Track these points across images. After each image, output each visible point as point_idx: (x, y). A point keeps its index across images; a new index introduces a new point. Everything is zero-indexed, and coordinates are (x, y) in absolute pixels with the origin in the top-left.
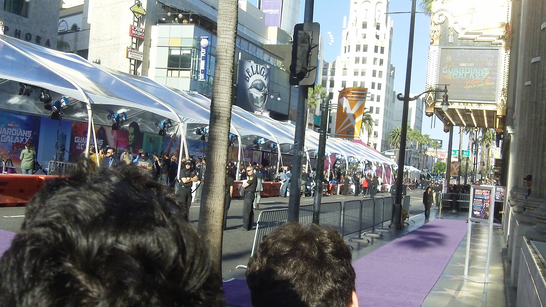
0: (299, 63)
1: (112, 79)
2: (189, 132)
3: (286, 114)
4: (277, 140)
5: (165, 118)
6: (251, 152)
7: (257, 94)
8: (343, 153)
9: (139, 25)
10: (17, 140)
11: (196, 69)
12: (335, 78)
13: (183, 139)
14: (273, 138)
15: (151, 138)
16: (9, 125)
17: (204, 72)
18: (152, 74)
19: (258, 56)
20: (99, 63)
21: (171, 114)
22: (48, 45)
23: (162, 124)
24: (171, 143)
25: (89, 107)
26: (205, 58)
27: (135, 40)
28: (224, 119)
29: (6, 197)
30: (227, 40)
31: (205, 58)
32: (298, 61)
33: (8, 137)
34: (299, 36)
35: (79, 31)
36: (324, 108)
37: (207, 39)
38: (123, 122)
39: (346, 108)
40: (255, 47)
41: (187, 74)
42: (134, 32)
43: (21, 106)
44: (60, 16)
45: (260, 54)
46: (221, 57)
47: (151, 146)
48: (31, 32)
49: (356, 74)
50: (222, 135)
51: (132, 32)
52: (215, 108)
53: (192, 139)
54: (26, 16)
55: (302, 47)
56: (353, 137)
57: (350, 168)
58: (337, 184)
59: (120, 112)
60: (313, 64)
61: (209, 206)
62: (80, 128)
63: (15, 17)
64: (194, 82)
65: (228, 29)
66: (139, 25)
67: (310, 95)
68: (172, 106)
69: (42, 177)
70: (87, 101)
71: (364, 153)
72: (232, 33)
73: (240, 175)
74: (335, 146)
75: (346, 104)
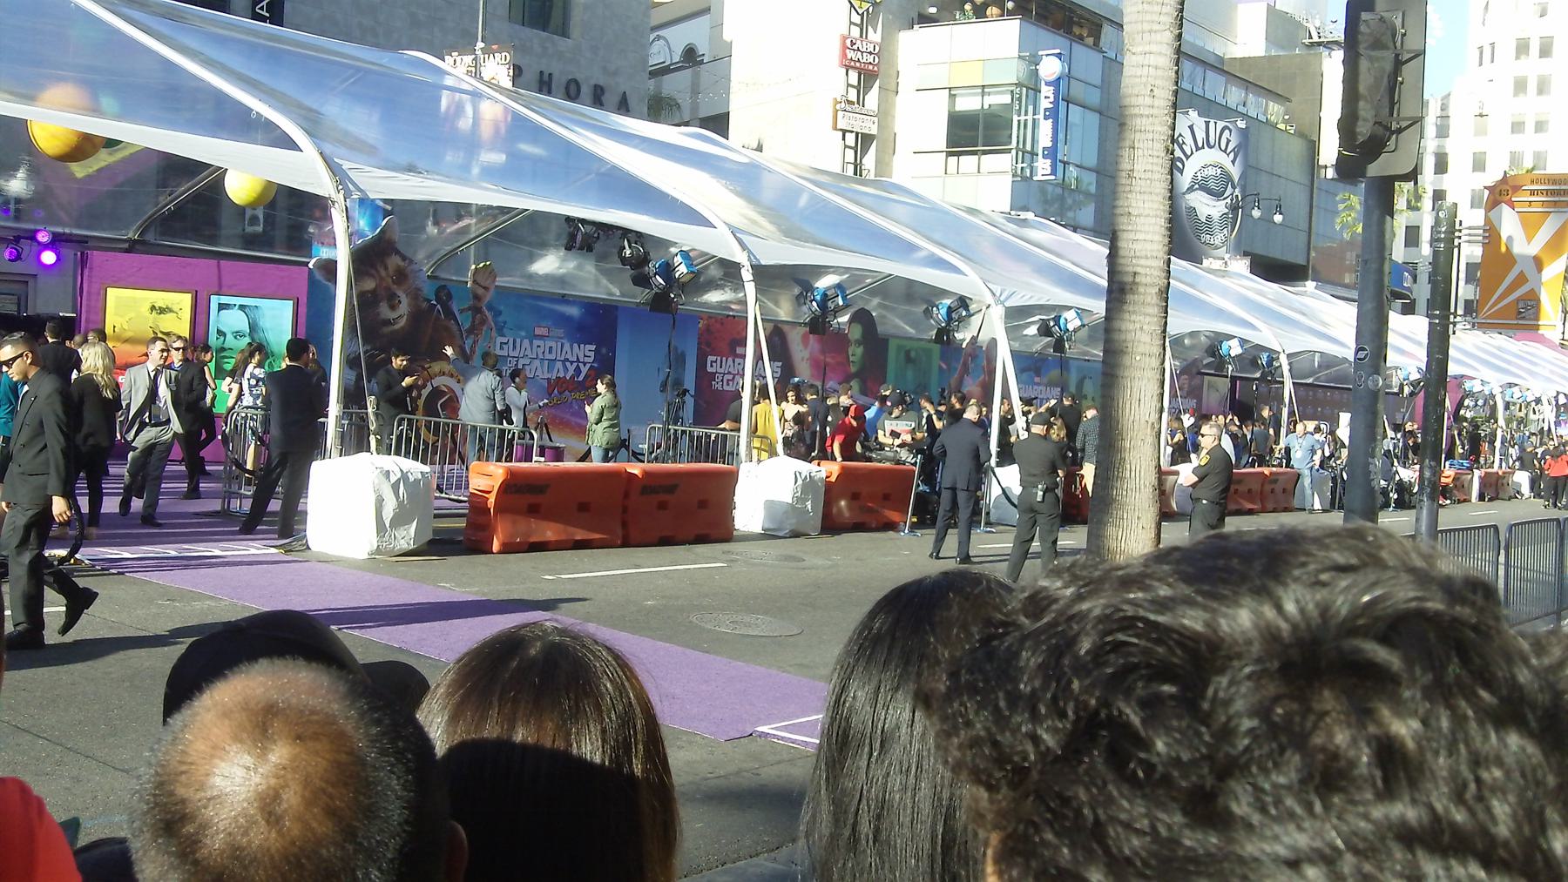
0: (1365, 110)
1: (800, 190)
2: (1013, 331)
3: (1301, 261)
4: (1281, 341)
5: (944, 293)
6: (1197, 381)
7: (1208, 207)
8: (1485, 373)
9: (863, 34)
10: (559, 371)
11: (1028, 148)
12: (1451, 146)
13: (1004, 356)
14: (1267, 336)
15: (908, 353)
16: (538, 331)
17: (1051, 153)
18: (904, 169)
19: (1209, 95)
20: (760, 149)
21: (966, 281)
22: (624, 107)
23: (943, 311)
24: (965, 364)
25: (747, 275)
26: (1052, 114)
27: (853, 77)
28: (1146, 297)
29: (545, 524)
30: (1152, 60)
31: (1052, 114)
32: (1361, 104)
33: (537, 363)
34: (1363, 28)
35: (702, 62)
36: (1439, 240)
37: (1059, 56)
38: (837, 311)
39: (1510, 238)
40: (1199, 70)
41: (1001, 164)
42: (850, 54)
43: (561, 280)
44: (654, 23)
45: (1214, 87)
46: (1136, 111)
47: (910, 374)
48: (579, 77)
49: (1517, 127)
50: (1146, 338)
51: (845, 55)
52: (1122, 261)
53: (1023, 349)
54: (564, 32)
55: (1371, 59)
56: (1537, 327)
57: (1508, 421)
58: (1471, 469)
59: (824, 283)
60: (1407, 109)
61: (1112, 544)
62: (723, 334)
63: (534, 36)
64: (1023, 181)
65: (1156, 27)
66: (863, 34)
67: (1400, 203)
68: (967, 259)
69: (635, 469)
70: (740, 257)
71: (1552, 372)
72: (1168, 37)
73: (1170, 450)
74: (1480, 358)
75: (1509, 224)
